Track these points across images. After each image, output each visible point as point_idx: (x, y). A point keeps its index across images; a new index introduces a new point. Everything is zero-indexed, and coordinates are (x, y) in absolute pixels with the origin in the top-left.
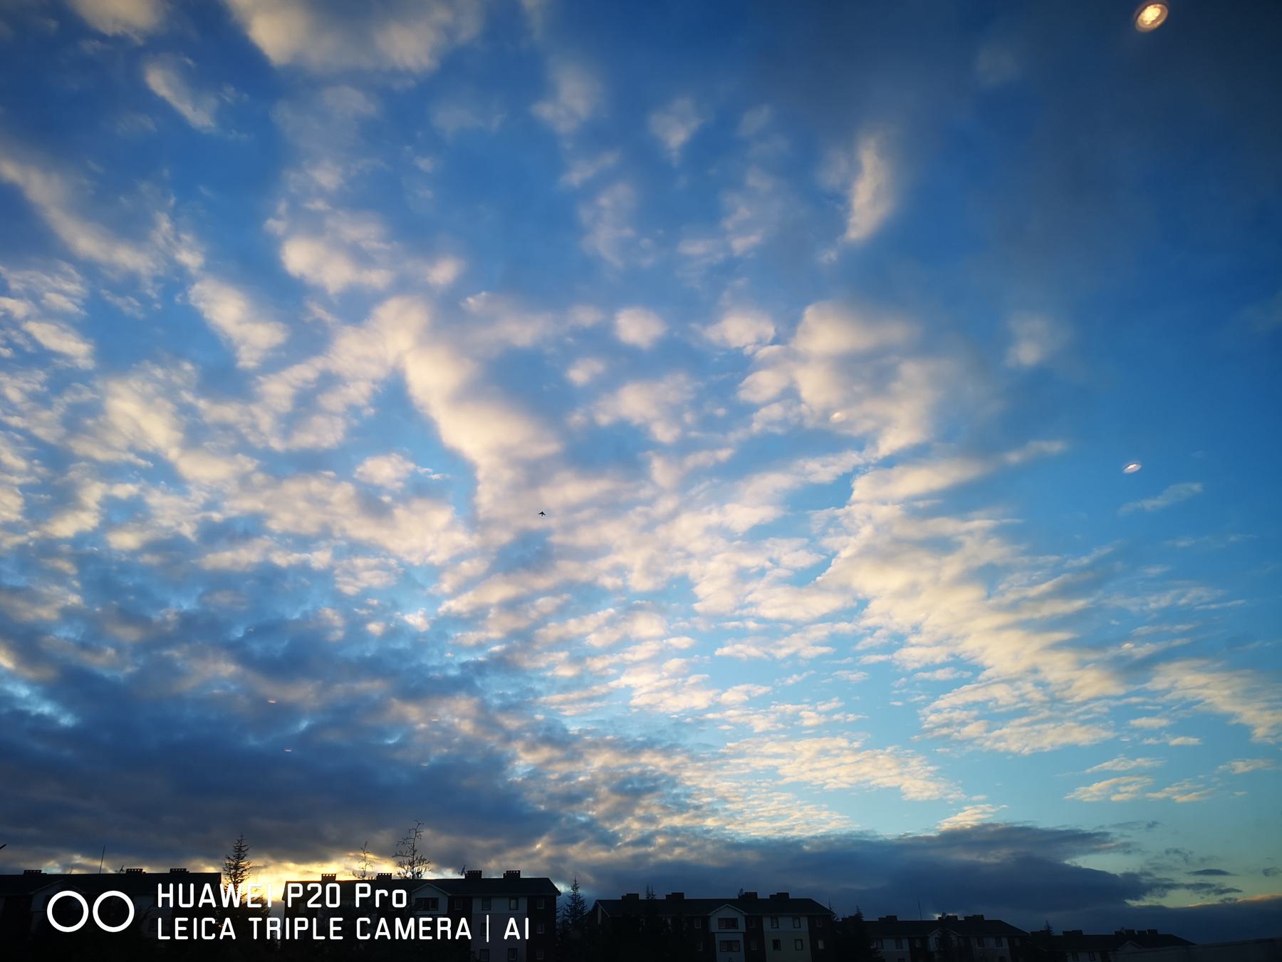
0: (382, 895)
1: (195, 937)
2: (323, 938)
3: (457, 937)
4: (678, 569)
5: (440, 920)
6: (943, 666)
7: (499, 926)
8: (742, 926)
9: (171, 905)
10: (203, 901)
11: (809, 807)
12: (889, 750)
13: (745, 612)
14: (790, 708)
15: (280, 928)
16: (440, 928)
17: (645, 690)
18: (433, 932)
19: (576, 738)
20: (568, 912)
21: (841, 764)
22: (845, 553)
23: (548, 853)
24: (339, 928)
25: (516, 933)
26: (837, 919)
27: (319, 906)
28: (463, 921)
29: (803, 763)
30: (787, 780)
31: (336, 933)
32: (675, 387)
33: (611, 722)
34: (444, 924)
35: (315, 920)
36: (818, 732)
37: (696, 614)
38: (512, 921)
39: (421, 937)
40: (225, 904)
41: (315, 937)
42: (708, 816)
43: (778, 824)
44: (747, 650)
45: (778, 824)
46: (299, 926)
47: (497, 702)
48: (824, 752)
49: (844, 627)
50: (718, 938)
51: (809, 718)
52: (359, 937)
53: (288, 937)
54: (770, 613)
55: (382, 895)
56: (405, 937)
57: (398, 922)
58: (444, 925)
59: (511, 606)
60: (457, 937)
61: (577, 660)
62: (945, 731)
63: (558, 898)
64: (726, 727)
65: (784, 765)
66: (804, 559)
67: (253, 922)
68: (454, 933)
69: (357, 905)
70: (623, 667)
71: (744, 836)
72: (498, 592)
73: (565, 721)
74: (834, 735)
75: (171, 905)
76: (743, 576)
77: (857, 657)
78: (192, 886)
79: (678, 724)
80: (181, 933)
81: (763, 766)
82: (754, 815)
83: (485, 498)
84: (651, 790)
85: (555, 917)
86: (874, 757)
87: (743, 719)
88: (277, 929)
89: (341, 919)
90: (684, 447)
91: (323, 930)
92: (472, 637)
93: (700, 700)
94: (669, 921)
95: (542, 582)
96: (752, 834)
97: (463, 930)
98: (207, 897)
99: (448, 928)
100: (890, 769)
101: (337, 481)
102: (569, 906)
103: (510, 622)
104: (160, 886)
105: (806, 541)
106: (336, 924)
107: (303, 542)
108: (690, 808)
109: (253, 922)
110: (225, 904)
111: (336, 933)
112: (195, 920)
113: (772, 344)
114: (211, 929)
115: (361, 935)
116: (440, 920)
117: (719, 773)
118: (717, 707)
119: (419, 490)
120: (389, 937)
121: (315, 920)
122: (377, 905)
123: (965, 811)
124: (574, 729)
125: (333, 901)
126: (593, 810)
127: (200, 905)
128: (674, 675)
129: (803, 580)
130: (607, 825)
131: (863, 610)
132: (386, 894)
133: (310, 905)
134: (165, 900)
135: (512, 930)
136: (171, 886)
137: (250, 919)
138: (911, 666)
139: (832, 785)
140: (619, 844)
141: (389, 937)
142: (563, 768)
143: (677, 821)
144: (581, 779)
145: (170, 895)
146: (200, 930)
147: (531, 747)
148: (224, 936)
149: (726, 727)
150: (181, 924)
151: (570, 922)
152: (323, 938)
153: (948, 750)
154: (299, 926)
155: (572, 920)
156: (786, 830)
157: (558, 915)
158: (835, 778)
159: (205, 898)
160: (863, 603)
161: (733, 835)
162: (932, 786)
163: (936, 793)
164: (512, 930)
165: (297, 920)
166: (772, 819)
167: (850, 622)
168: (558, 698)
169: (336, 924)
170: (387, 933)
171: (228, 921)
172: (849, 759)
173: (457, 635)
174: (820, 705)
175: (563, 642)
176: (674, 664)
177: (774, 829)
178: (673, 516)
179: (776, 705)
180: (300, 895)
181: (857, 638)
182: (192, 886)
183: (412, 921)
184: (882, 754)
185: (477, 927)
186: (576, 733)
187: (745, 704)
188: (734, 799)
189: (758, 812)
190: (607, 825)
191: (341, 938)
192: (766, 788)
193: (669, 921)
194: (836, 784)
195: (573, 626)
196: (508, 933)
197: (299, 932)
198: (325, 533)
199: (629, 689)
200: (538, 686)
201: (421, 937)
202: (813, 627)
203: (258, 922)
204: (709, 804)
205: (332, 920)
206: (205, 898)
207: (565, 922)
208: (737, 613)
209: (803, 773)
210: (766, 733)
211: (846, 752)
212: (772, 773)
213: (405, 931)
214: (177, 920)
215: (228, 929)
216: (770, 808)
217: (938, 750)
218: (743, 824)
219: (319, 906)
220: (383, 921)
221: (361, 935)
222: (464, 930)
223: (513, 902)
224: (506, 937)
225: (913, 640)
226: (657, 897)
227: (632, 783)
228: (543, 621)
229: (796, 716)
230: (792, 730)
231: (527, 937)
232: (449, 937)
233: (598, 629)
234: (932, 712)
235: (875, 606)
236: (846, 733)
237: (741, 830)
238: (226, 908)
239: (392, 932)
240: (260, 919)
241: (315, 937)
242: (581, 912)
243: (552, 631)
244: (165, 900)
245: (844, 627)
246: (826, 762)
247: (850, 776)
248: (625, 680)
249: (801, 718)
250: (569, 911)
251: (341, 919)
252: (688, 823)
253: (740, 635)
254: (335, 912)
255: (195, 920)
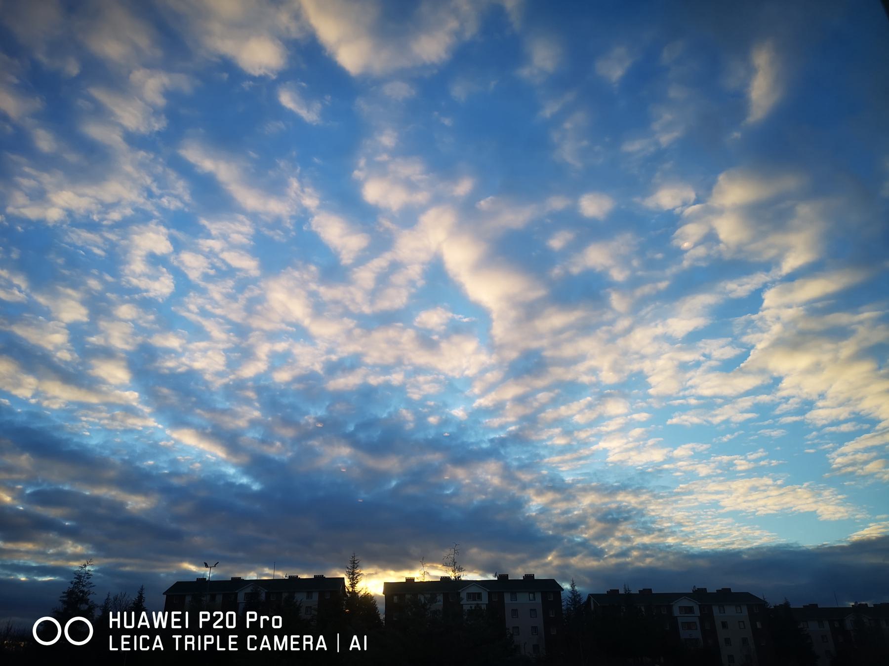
0: (265, 620)
1: (135, 649)
2: (224, 649)
3: (317, 649)
4: (635, 367)
5: (305, 637)
6: (846, 421)
7: (346, 642)
8: (697, 612)
9: (119, 627)
10: (140, 623)
11: (745, 528)
12: (805, 485)
13: (687, 393)
14: (725, 458)
15: (194, 643)
16: (305, 643)
17: (617, 450)
18: (300, 645)
19: (570, 486)
20: (570, 602)
21: (769, 497)
22: (760, 346)
23: (556, 562)
24: (235, 643)
25: (358, 646)
26: (770, 607)
27: (221, 627)
28: (321, 637)
29: (738, 497)
30: (727, 509)
31: (233, 646)
32: (624, 242)
33: (595, 474)
34: (308, 640)
35: (218, 637)
36: (749, 474)
37: (651, 396)
38: (355, 637)
39: (292, 649)
40: (156, 626)
41: (219, 649)
42: (669, 536)
43: (719, 541)
44: (691, 419)
45: (722, 540)
46: (207, 641)
47: (515, 463)
48: (754, 489)
49: (764, 398)
50: (680, 620)
51: (741, 465)
52: (249, 649)
53: (199, 649)
54: (707, 392)
55: (265, 620)
56: (281, 648)
57: (276, 638)
58: (308, 641)
59: (520, 400)
60: (317, 649)
61: (567, 433)
62: (850, 469)
63: (562, 592)
64: (678, 474)
65: (723, 498)
66: (729, 352)
67: (175, 638)
68: (315, 646)
69: (248, 627)
70: (600, 436)
71: (696, 549)
72: (512, 391)
73: (562, 474)
74: (761, 476)
75: (119, 627)
76: (684, 367)
77: (777, 419)
78: (133, 613)
79: (643, 473)
80: (126, 646)
81: (708, 500)
82: (703, 534)
83: (499, 330)
84: (626, 519)
85: (561, 606)
86: (794, 490)
87: (690, 468)
88: (192, 643)
89: (236, 636)
90: (634, 283)
91: (224, 643)
92: (496, 422)
93: (657, 456)
94: (643, 609)
95: (540, 383)
96: (703, 547)
97: (321, 644)
98: (144, 621)
99: (311, 643)
100: (807, 499)
101: (403, 329)
102: (570, 598)
103: (521, 410)
104: (111, 613)
105: (730, 339)
106: (233, 640)
107: (386, 369)
108: (655, 531)
109: (175, 638)
110: (156, 626)
111: (233, 646)
112: (135, 637)
113: (694, 204)
114: (146, 643)
115: (250, 647)
116: (305, 637)
117: (675, 506)
118: (670, 460)
119: (455, 330)
120: (270, 649)
121: (218, 637)
122: (262, 626)
123: (870, 527)
124: (568, 479)
125: (231, 623)
126: (586, 534)
127: (139, 627)
128: (637, 440)
129: (729, 367)
130: (596, 543)
131: (778, 385)
132: (268, 619)
133: (215, 626)
134: (115, 623)
135: (355, 643)
136: (119, 613)
137: (174, 636)
138: (820, 423)
139: (762, 512)
140: (606, 556)
141: (270, 649)
142: (563, 506)
143: (646, 540)
144: (576, 513)
145: (118, 620)
146: (139, 644)
147: (540, 493)
148: (156, 648)
149: (678, 474)
150: (125, 640)
151: (572, 609)
152: (224, 649)
153: (853, 483)
154: (207, 641)
155: (573, 607)
156: (728, 544)
157: (563, 604)
158: (764, 506)
159: (142, 622)
160: (777, 380)
161: (688, 549)
162: (842, 509)
163: (846, 514)
164: (355, 643)
165: (206, 637)
166: (717, 537)
167: (768, 394)
168: (557, 459)
169: (233, 640)
170: (268, 646)
171: (158, 637)
172: (775, 493)
173: (486, 421)
174: (750, 455)
175: (557, 422)
176: (637, 432)
177: (719, 544)
178: (629, 331)
179: (715, 457)
180: (208, 619)
181: (774, 406)
182: (133, 613)
183: (285, 638)
184: (800, 488)
185: (330, 642)
186: (570, 482)
187: (691, 457)
188: (687, 524)
189: (706, 533)
190: (596, 543)
191: (236, 649)
192: (711, 515)
193: (643, 609)
194: (765, 511)
195: (563, 410)
196: (352, 646)
197: (208, 645)
198: (399, 362)
199: (606, 451)
200: (542, 452)
201: (292, 649)
202: (740, 400)
203: (179, 638)
204: (669, 527)
205: (230, 637)
206: (142, 622)
207: (568, 609)
208: (681, 394)
209: (739, 504)
210: (709, 477)
211: (771, 488)
212: (715, 505)
213: (281, 644)
214: (123, 637)
215: (158, 644)
216: (715, 529)
217: (845, 483)
218: (694, 541)
219: (221, 627)
220: (265, 637)
221: (250, 647)
222: (322, 644)
223: (531, 595)
224: (351, 649)
225: (820, 404)
226: (632, 592)
227: (612, 515)
228: (542, 408)
229: (731, 464)
230: (728, 473)
231: (365, 649)
232: (312, 649)
233: (581, 411)
234: (839, 456)
235: (785, 384)
236: (771, 474)
237: (693, 544)
238: (164, 629)
239: (272, 645)
240: (180, 636)
241: (219, 649)
242: (579, 602)
243: (550, 414)
244: (115, 623)
245: (764, 398)
246: (755, 496)
247: (776, 505)
248: (602, 445)
249: (735, 465)
250: (571, 601)
251: (236, 636)
252: (654, 541)
253: (684, 409)
254: (232, 632)
255: (135, 637)
